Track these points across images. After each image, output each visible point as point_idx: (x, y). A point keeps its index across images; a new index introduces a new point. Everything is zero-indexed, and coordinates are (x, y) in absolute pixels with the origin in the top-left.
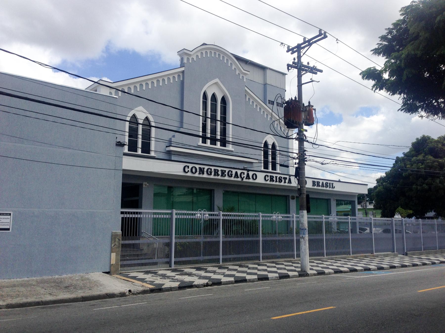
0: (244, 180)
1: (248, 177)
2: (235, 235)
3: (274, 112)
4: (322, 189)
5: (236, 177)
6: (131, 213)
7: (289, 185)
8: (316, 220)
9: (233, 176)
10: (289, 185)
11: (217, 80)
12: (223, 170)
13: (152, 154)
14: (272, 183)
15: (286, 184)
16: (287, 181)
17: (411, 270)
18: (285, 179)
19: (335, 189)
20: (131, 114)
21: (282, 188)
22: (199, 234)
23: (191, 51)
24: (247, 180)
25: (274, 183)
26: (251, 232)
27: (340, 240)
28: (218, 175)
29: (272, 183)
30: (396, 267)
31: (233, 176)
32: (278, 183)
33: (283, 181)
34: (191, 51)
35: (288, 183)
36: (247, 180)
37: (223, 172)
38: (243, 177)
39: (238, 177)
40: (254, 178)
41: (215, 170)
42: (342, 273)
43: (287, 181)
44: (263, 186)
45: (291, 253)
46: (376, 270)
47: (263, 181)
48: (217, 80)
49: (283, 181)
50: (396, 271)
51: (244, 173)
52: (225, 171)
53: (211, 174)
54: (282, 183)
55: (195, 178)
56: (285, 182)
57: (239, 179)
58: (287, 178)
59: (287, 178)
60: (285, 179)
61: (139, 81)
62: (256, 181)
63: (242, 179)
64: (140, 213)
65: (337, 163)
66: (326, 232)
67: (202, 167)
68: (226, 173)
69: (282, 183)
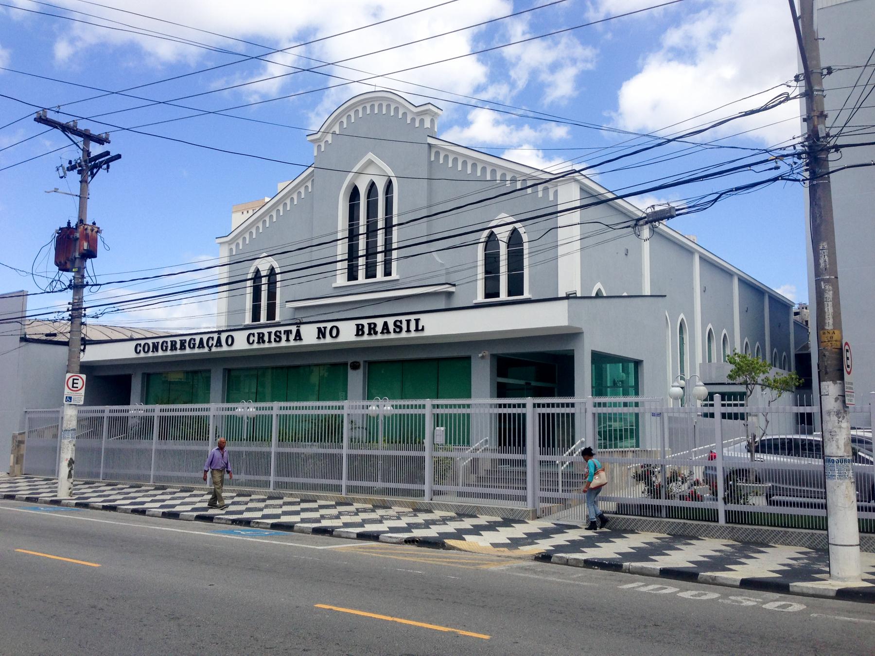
0: (214, 349)
1: (385, 329)
2: (560, 447)
3: (857, 83)
4: (261, 348)
5: (297, 340)
6: (451, 406)
7: (298, 343)
8: (320, 412)
9: (197, 345)
10: (298, 343)
11: (371, 156)
12: (183, 340)
13: (527, 295)
14: (262, 346)
15: (292, 343)
16: (292, 337)
17: (20, 507)
18: (288, 333)
19: (426, 333)
20: (252, 269)
21: (188, 358)
22: (460, 444)
23: (429, 103)
24: (219, 349)
25: (267, 345)
26: (178, 436)
27: (197, 451)
28: (376, 333)
29: (262, 346)
30: (214, 521)
31: (169, 348)
32: (274, 345)
33: (284, 337)
34: (416, 107)
35: (295, 339)
36: (219, 349)
37: (398, 327)
38: (210, 345)
39: (203, 347)
40: (230, 343)
41: (153, 343)
42: (88, 508)
43: (292, 337)
44: (247, 354)
45: (263, 478)
46: (159, 517)
47: (315, 341)
48: (371, 156)
49: (284, 337)
50: (114, 519)
51: (213, 338)
52: (185, 340)
53: (166, 350)
54: (404, 335)
55: (218, 354)
56: (288, 340)
57: (206, 350)
58: (291, 331)
59: (291, 331)
60: (288, 333)
61: (500, 166)
62: (340, 339)
63: (210, 348)
64: (469, 406)
65: (120, 308)
66: (802, 449)
67: (155, 341)
68: (187, 345)
69: (283, 343)
